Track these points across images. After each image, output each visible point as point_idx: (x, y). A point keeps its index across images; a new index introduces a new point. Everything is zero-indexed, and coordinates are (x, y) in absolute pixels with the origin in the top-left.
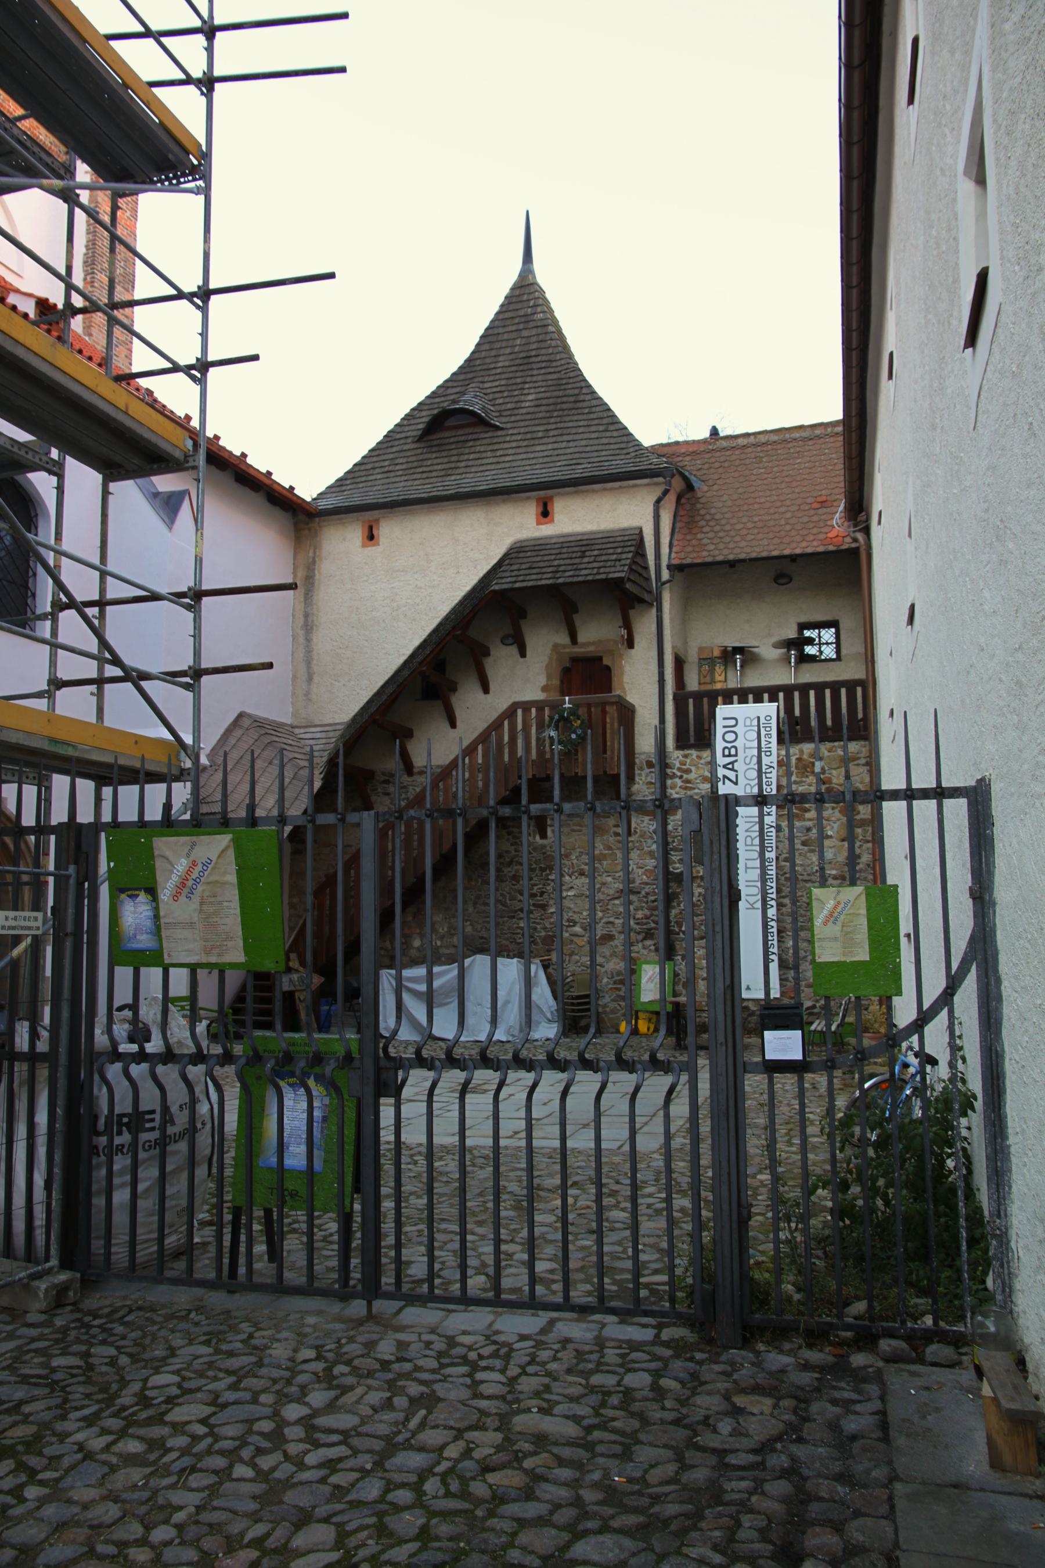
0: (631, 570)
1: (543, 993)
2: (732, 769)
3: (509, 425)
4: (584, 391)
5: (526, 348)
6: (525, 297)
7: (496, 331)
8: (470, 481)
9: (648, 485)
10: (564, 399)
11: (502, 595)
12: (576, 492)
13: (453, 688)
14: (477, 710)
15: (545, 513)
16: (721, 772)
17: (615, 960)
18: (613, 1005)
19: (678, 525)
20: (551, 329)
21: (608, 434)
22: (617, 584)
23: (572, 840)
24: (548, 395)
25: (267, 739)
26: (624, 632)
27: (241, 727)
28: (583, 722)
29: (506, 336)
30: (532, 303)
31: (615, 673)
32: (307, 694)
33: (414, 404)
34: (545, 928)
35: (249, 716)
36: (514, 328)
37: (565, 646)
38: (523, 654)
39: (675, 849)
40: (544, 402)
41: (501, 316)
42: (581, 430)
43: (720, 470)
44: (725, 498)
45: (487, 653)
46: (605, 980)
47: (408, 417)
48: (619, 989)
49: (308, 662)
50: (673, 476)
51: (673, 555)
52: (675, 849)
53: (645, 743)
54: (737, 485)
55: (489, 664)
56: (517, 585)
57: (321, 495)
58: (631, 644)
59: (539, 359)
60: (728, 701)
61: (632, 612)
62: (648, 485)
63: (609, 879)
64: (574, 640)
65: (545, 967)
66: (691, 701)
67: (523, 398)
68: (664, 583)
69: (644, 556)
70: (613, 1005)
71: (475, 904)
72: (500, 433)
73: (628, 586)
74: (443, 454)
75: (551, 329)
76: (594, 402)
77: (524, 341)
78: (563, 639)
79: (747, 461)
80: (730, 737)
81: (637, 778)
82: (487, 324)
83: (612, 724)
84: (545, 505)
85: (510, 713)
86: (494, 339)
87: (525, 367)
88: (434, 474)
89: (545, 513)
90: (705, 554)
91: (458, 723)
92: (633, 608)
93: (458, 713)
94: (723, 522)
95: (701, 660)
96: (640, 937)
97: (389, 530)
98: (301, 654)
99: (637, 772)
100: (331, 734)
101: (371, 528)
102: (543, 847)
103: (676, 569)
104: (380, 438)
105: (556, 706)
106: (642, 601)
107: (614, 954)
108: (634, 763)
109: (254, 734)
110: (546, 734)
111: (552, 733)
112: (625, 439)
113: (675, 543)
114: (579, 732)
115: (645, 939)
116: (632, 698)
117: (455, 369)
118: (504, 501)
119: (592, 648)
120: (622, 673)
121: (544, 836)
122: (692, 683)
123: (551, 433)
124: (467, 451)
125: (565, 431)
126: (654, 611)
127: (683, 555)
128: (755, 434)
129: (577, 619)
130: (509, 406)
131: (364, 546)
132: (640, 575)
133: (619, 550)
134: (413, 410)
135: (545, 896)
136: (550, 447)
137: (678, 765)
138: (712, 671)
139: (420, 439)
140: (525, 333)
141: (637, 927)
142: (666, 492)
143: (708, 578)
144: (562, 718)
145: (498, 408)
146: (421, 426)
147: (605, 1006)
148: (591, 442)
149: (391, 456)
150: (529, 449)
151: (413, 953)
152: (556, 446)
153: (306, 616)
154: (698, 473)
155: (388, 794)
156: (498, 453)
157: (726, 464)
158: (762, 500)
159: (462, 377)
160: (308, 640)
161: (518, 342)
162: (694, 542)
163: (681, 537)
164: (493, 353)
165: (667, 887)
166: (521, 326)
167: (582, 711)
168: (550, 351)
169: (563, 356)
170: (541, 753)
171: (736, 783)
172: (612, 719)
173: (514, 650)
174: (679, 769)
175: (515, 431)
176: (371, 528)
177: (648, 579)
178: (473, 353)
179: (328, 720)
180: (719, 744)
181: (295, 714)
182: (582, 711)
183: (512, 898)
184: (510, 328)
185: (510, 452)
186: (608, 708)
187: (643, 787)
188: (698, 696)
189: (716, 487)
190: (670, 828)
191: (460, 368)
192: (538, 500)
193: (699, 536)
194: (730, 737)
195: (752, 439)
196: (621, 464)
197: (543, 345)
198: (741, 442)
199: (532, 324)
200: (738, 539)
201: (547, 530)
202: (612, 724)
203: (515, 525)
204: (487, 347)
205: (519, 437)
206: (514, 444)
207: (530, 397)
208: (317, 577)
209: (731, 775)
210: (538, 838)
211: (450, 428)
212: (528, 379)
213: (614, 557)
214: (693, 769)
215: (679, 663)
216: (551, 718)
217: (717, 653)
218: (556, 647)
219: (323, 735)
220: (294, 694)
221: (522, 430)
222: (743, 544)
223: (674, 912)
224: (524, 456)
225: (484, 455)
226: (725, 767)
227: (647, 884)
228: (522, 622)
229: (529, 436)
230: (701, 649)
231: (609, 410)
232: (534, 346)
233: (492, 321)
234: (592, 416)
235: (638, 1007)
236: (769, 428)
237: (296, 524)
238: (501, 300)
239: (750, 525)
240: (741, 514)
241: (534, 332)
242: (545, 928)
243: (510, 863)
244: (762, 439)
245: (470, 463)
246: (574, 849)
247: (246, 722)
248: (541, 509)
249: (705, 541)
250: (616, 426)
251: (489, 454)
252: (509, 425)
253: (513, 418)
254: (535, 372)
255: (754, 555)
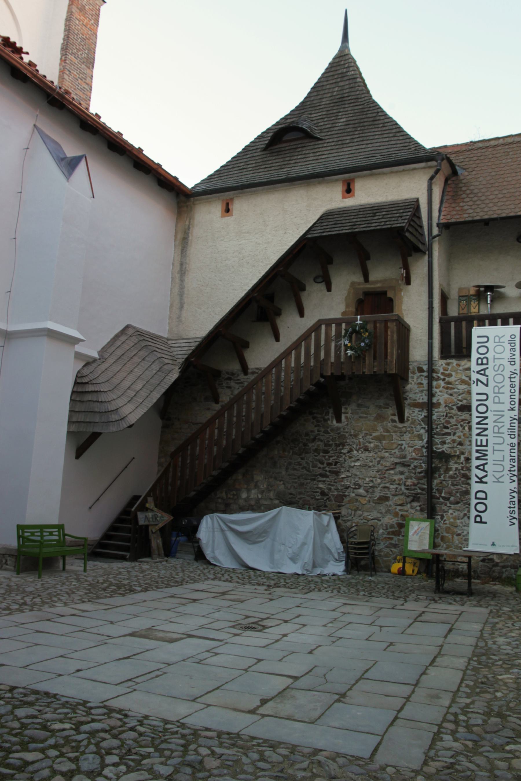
0: (410, 224)
1: (333, 540)
2: (484, 375)
3: (326, 137)
4: (380, 114)
5: (341, 92)
6: (342, 63)
7: (321, 84)
8: (298, 169)
9: (424, 168)
10: (366, 120)
11: (315, 240)
12: (372, 175)
13: (278, 313)
14: (293, 326)
15: (349, 191)
16: (474, 376)
17: (389, 516)
18: (386, 550)
19: (445, 198)
20: (359, 80)
21: (396, 138)
22: (400, 231)
23: (360, 424)
24: (355, 118)
25: (144, 344)
26: (403, 272)
27: (126, 334)
28: (370, 333)
29: (328, 87)
30: (346, 66)
31: (396, 303)
32: (179, 317)
33: (264, 130)
34: (337, 489)
35: (134, 328)
36: (334, 81)
37: (359, 284)
38: (329, 289)
39: (437, 434)
40: (352, 122)
41: (326, 75)
42: (377, 137)
43: (477, 162)
44: (481, 179)
45: (303, 289)
46: (381, 531)
47: (260, 137)
48: (391, 539)
49: (181, 295)
50: (442, 160)
51: (442, 217)
52: (437, 434)
53: (418, 353)
54: (490, 170)
55: (304, 297)
56: (325, 234)
57: (196, 186)
58: (408, 281)
59: (350, 98)
60: (481, 324)
61: (410, 259)
62: (424, 168)
63: (387, 454)
64: (366, 280)
65: (336, 518)
66: (453, 324)
67: (337, 121)
68: (435, 237)
69: (420, 218)
70: (386, 550)
71: (287, 469)
72: (320, 142)
73: (407, 234)
74: (280, 157)
75: (359, 80)
76: (387, 120)
77: (340, 88)
78: (358, 278)
79: (498, 155)
80: (483, 350)
81: (410, 380)
82: (316, 80)
83: (392, 336)
84: (349, 185)
85: (316, 328)
86: (320, 89)
87: (340, 103)
88: (273, 168)
89: (349, 191)
90: (466, 216)
91: (281, 338)
92: (410, 255)
93: (281, 331)
94: (480, 195)
95: (461, 297)
96: (409, 500)
97: (242, 206)
98: (176, 290)
99: (410, 375)
100: (192, 344)
101: (228, 204)
102: (338, 428)
103: (445, 227)
104: (240, 150)
105: (350, 323)
106: (417, 250)
107: (388, 511)
108: (408, 369)
109: (135, 339)
110: (342, 342)
111: (347, 342)
112: (408, 141)
113: (443, 209)
114: (367, 341)
115: (413, 501)
116: (408, 320)
117: (293, 108)
118: (320, 183)
119: (379, 285)
120: (401, 303)
121: (339, 420)
122: (453, 311)
123: (355, 140)
124: (297, 154)
125: (365, 138)
126: (426, 258)
127: (449, 217)
128: (503, 138)
129: (369, 264)
130: (327, 126)
131: (223, 216)
132: (417, 230)
133: (401, 211)
134: (263, 133)
135: (338, 465)
136: (354, 148)
137: (442, 371)
138: (468, 305)
139: (265, 149)
140: (341, 84)
141: (407, 492)
142: (437, 172)
143: (468, 234)
144: (354, 331)
145: (320, 128)
146: (267, 142)
147: (380, 551)
148: (383, 144)
149: (245, 160)
150: (339, 150)
151: (241, 502)
152: (358, 147)
153: (182, 264)
154: (461, 164)
155: (229, 387)
156: (318, 154)
157: (482, 158)
158: (510, 179)
159: (297, 112)
160: (182, 281)
161: (336, 89)
162: (457, 208)
163: (447, 205)
164: (319, 97)
165: (430, 462)
166: (339, 80)
167: (370, 327)
168: (358, 93)
169: (366, 95)
170: (338, 356)
171: (487, 385)
172: (392, 332)
173: (322, 286)
174: (443, 374)
175: (331, 140)
176: (228, 204)
177: (422, 235)
178: (306, 98)
179: (192, 335)
180: (474, 355)
181: (170, 331)
182: (370, 327)
183: (314, 466)
184: (331, 82)
185: (326, 152)
186: (389, 324)
187: (415, 389)
188: (458, 320)
189: (474, 173)
190: (434, 417)
191: (297, 107)
192: (344, 181)
193: (461, 204)
194: (483, 350)
195: (501, 141)
196: (403, 155)
197: (353, 90)
198: (493, 143)
199: (346, 78)
200: (491, 205)
201: (350, 202)
202: (392, 336)
203: (328, 199)
204: (315, 94)
205: (333, 144)
206: (329, 148)
207: (342, 120)
208: (190, 238)
209: (483, 379)
210: (335, 422)
211: (287, 141)
212: (342, 110)
213: (398, 215)
214: (453, 373)
215: (444, 299)
216: (346, 331)
217: (472, 292)
218: (353, 284)
219: (187, 345)
220: (170, 317)
221: (335, 140)
222: (495, 208)
223: (435, 482)
224: (336, 155)
225: (308, 155)
226: (478, 372)
227: (415, 459)
228: (330, 267)
229: (340, 143)
230: (460, 289)
231: (397, 124)
232: (347, 91)
233: (320, 79)
234: (384, 128)
235: (406, 554)
236: (514, 133)
237: (178, 203)
238: (326, 65)
239: (500, 196)
240: (493, 189)
241: (347, 82)
242: (337, 489)
243: (314, 440)
244: (510, 140)
245: (298, 161)
246: (361, 431)
247: (130, 332)
248: (345, 188)
249: (466, 207)
250: (402, 134)
251: (311, 155)
252: (326, 137)
253: (329, 133)
254: (346, 106)
255: (504, 215)
